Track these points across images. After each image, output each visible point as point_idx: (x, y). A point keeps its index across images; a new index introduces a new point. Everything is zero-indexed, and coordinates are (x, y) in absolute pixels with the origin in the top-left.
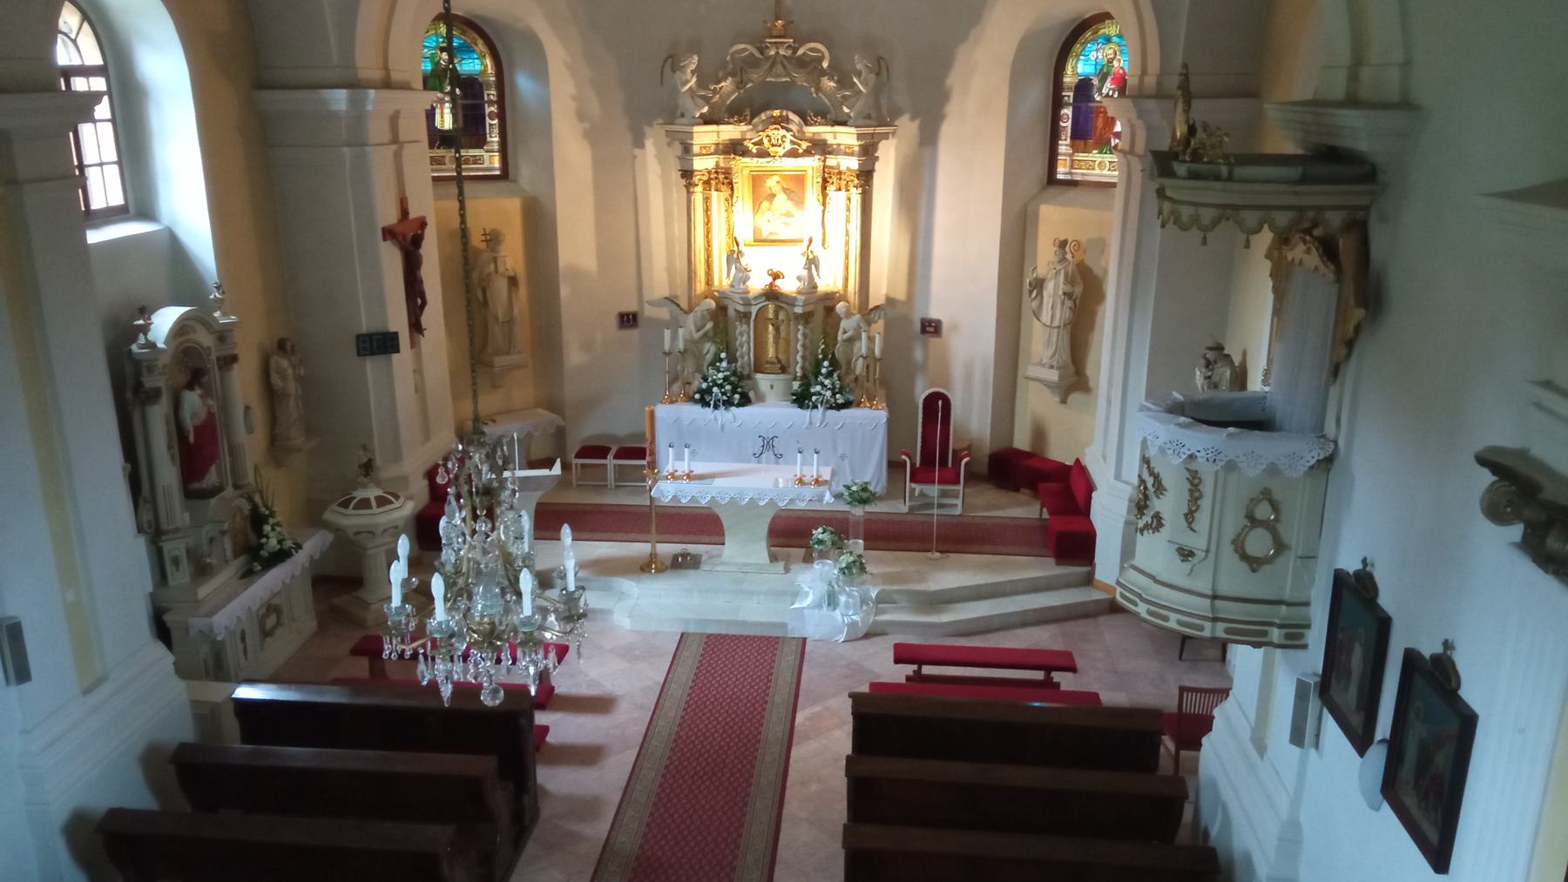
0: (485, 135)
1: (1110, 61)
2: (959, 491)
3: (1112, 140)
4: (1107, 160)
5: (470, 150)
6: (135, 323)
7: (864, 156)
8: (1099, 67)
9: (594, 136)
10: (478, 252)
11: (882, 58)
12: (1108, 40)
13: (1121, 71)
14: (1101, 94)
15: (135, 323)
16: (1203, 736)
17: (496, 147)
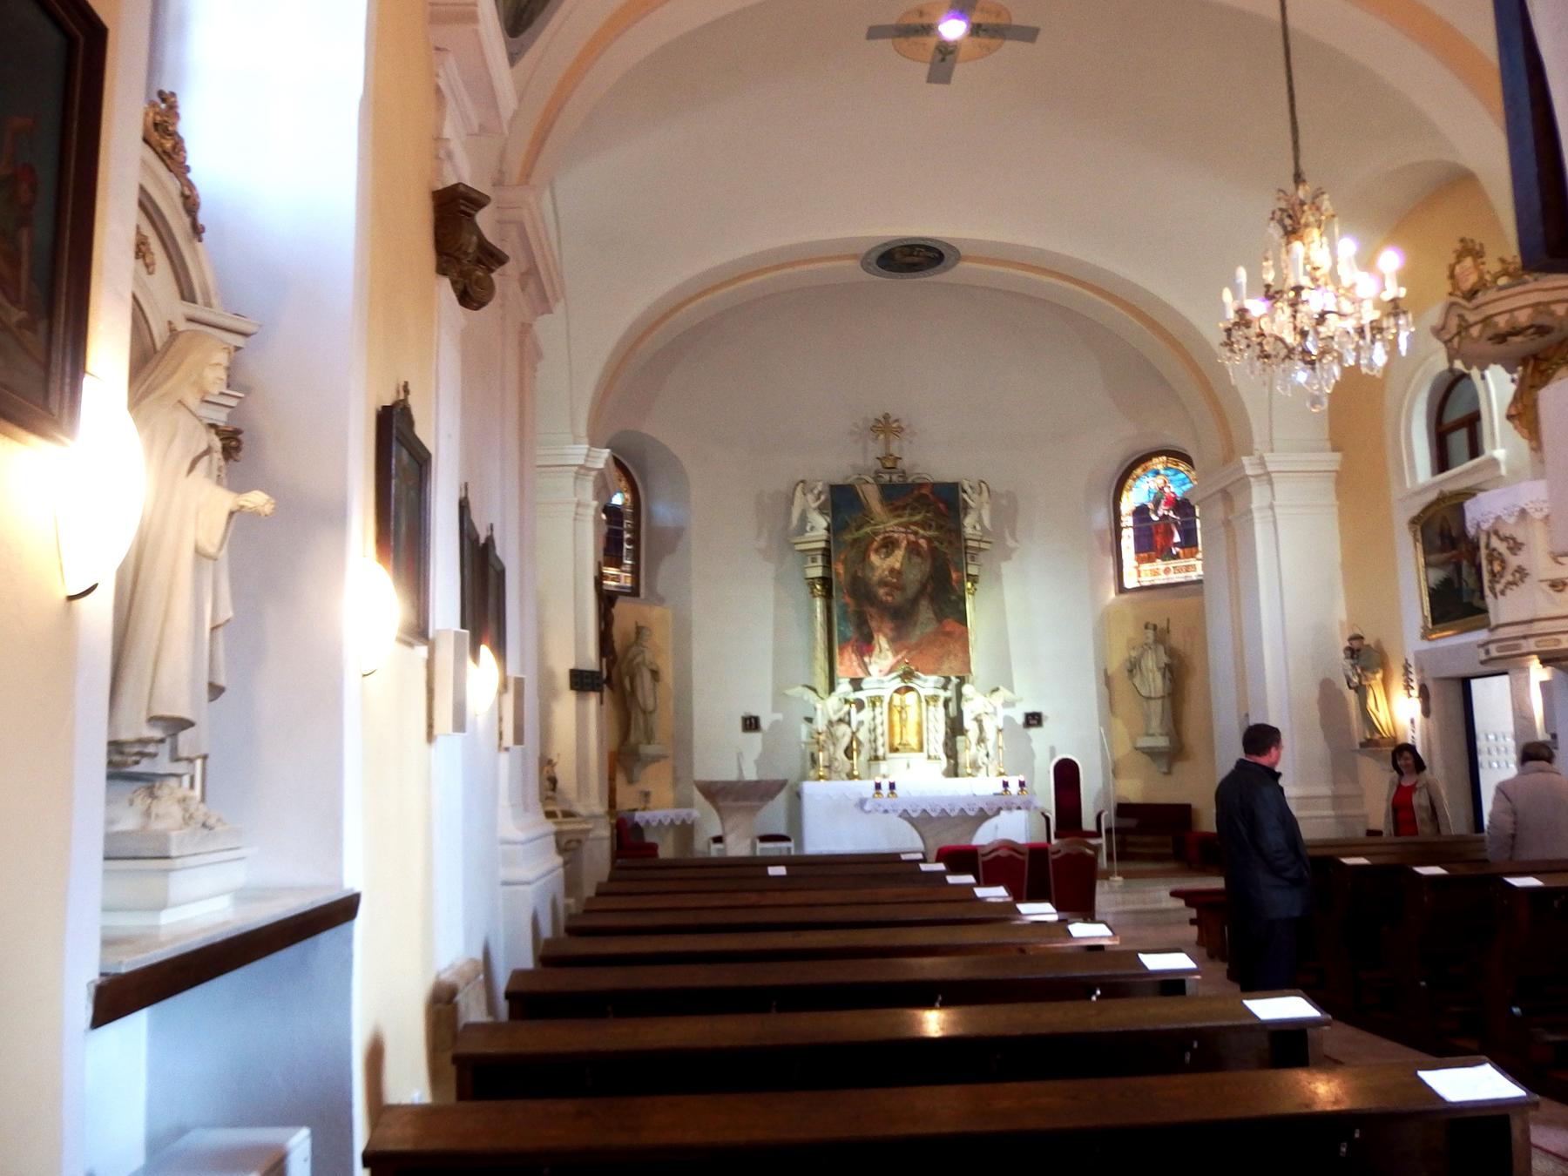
0: (622, 557)
1: (1161, 489)
2: (1100, 845)
3: (1173, 549)
4: (1171, 566)
5: (1428, 599)
6: (1404, 353)
7: (1442, 550)
8: (1152, 496)
9: (1070, 942)
10: (821, 510)
11: (983, 482)
12: (1157, 473)
13: (1172, 495)
14: (1157, 515)
15: (1404, 353)
16: (1441, 1099)
17: (628, 568)
